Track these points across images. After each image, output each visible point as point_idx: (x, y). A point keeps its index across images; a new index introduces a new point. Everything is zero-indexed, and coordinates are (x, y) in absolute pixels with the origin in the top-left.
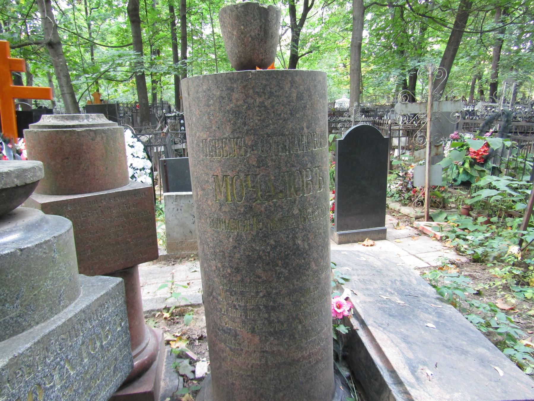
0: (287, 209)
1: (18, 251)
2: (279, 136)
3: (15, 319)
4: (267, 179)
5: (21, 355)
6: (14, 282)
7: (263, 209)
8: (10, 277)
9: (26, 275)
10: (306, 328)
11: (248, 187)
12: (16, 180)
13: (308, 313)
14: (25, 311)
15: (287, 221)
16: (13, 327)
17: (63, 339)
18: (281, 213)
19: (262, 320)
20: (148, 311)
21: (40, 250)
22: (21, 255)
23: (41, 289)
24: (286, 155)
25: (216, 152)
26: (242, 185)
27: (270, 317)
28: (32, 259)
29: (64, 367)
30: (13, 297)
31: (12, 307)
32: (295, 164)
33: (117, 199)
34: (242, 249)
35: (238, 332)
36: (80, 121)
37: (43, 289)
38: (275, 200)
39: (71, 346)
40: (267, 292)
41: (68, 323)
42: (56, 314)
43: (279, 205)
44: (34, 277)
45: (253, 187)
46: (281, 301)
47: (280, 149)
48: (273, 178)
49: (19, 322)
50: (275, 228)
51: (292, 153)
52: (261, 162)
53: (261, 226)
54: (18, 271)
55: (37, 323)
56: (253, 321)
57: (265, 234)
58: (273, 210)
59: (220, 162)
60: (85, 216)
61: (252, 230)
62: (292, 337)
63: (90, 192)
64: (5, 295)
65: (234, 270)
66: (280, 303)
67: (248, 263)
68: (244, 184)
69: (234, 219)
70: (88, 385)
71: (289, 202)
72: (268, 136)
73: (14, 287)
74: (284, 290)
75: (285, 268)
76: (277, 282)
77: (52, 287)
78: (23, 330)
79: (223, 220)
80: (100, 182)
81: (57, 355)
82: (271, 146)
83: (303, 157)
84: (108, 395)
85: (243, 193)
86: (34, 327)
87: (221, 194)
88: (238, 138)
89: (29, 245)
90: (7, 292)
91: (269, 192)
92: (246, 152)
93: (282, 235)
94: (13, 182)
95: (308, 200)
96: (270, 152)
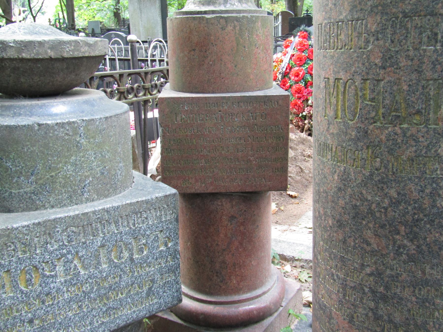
0: (426, 144)
1: (36, 125)
2: (425, 16)
3: (29, 195)
4: (395, 88)
5: (13, 229)
6: (30, 156)
7: (383, 137)
8: (26, 150)
9: (43, 153)
11: (365, 99)
12: (49, 51)
14: (40, 190)
15: (425, 165)
16: (27, 202)
17: (73, 232)
18: (414, 149)
19: (365, 309)
20: (306, 260)
21: (62, 130)
22: (38, 130)
23: (59, 173)
24: (436, 51)
25: (330, 42)
26: (357, 94)
27: (376, 308)
28: (50, 137)
29: (72, 262)
30: (28, 172)
31: (27, 181)
33: (242, 104)
34: (348, 193)
35: (333, 314)
36: (216, 7)
37: (62, 173)
38: (405, 126)
39: (84, 243)
40: (377, 269)
41: (82, 217)
42: (77, 204)
43: (412, 135)
44: (53, 157)
45: (372, 100)
46: (398, 291)
47: (425, 39)
48: (405, 87)
49: (32, 199)
50: (401, 172)
52: (389, 60)
53: (378, 164)
54: (35, 146)
55: (53, 207)
56: (353, 305)
57: (383, 178)
58: (399, 141)
59: (332, 57)
60: (202, 120)
61: (364, 168)
63: (213, 93)
64: (20, 167)
65: (335, 223)
66: (395, 294)
67: (354, 218)
68: (360, 94)
69: (342, 147)
70: (105, 294)
72: (405, 16)
73: (29, 161)
74: (404, 275)
75: (412, 241)
76: (395, 259)
77: (74, 174)
78: (37, 209)
79: (330, 146)
80: (226, 81)
81: (62, 245)
82: (408, 33)
85: (356, 108)
86: (48, 209)
87: (331, 106)
88: (358, 20)
89: (49, 122)
90: (23, 165)
91: (396, 110)
92: (367, 42)
93: (412, 186)
94: (46, 53)
96: (405, 44)
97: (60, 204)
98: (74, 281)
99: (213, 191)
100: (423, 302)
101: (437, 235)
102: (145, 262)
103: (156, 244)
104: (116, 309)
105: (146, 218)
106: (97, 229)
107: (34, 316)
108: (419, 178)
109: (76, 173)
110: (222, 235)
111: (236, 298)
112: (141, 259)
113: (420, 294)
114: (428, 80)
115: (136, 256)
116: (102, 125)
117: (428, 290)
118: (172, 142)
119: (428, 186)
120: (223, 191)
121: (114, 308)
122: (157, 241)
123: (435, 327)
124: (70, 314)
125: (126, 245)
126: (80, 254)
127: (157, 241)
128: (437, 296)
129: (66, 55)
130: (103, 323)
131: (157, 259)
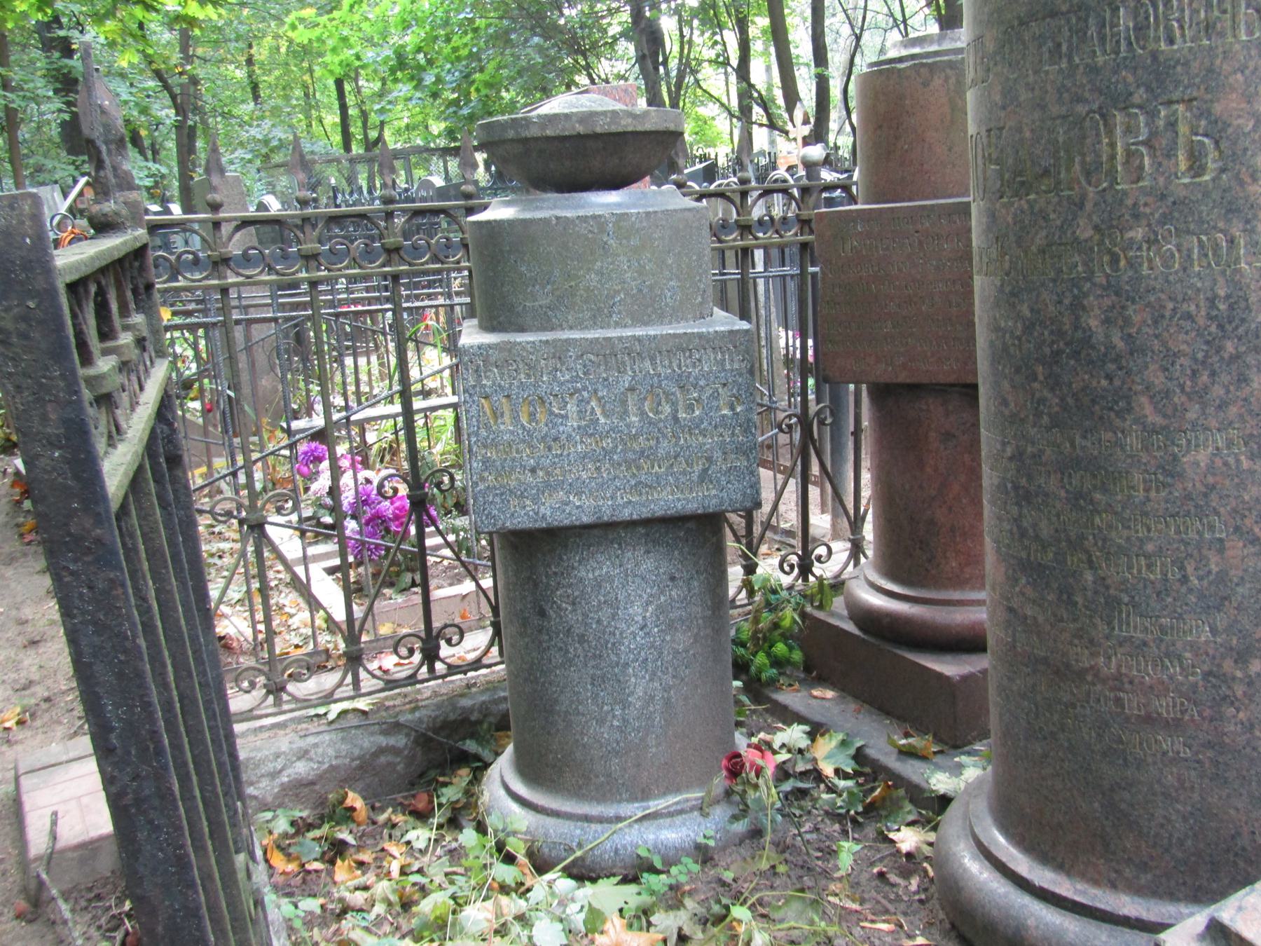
0: (1059, 223)
2: (1044, 19)
10: (1108, 588)
13: (1119, 546)
27: (1020, 515)
29: (588, 403)
32: (1087, 95)
33: (956, 217)
38: (1032, 197)
39: (606, 380)
44: (572, 260)
47: (1046, 56)
48: (1028, 135)
51: (1077, 60)
55: (571, 328)
60: (887, 249)
62: (1065, 597)
63: (910, 200)
70: (634, 460)
71: (1065, 203)
75: (1052, 390)
83: (1115, 72)
84: (679, 506)
89: (569, 215)
94: (574, 128)
95: (1129, 202)
97: (579, 325)
98: (589, 429)
99: (908, 381)
100: (1078, 499)
101: (1086, 377)
102: (694, 427)
103: (715, 403)
104: (650, 487)
105: (699, 360)
106: (623, 363)
107: (538, 464)
108: (1054, 281)
109: (602, 285)
110: (929, 470)
111: (956, 595)
112: (690, 421)
113: (1070, 484)
114: (1054, 119)
115: (682, 415)
116: (641, 222)
117: (1082, 477)
118: (837, 290)
119: (1067, 294)
120: (925, 380)
121: (647, 486)
122: (717, 398)
123: (1096, 544)
124: (584, 475)
125: (667, 394)
126: (600, 394)
127: (717, 398)
128: (1095, 487)
129: (598, 130)
130: (630, 502)
131: (716, 427)
